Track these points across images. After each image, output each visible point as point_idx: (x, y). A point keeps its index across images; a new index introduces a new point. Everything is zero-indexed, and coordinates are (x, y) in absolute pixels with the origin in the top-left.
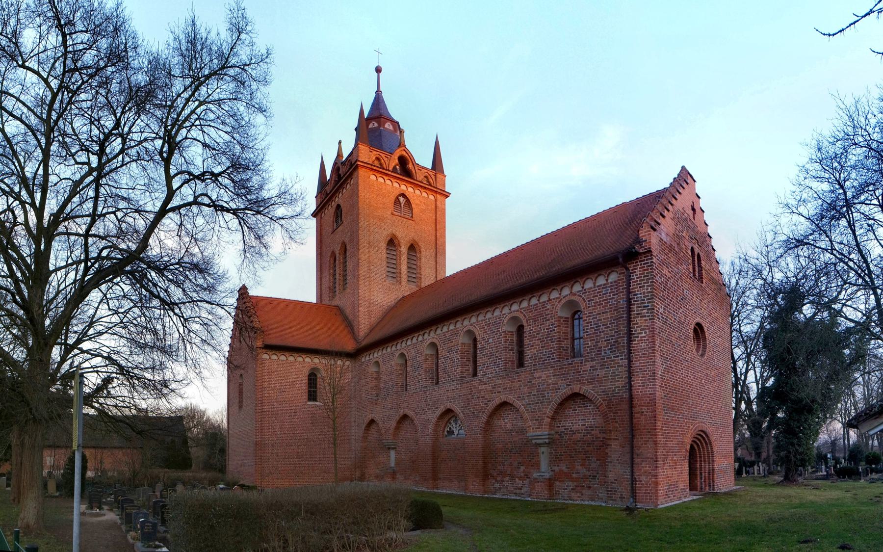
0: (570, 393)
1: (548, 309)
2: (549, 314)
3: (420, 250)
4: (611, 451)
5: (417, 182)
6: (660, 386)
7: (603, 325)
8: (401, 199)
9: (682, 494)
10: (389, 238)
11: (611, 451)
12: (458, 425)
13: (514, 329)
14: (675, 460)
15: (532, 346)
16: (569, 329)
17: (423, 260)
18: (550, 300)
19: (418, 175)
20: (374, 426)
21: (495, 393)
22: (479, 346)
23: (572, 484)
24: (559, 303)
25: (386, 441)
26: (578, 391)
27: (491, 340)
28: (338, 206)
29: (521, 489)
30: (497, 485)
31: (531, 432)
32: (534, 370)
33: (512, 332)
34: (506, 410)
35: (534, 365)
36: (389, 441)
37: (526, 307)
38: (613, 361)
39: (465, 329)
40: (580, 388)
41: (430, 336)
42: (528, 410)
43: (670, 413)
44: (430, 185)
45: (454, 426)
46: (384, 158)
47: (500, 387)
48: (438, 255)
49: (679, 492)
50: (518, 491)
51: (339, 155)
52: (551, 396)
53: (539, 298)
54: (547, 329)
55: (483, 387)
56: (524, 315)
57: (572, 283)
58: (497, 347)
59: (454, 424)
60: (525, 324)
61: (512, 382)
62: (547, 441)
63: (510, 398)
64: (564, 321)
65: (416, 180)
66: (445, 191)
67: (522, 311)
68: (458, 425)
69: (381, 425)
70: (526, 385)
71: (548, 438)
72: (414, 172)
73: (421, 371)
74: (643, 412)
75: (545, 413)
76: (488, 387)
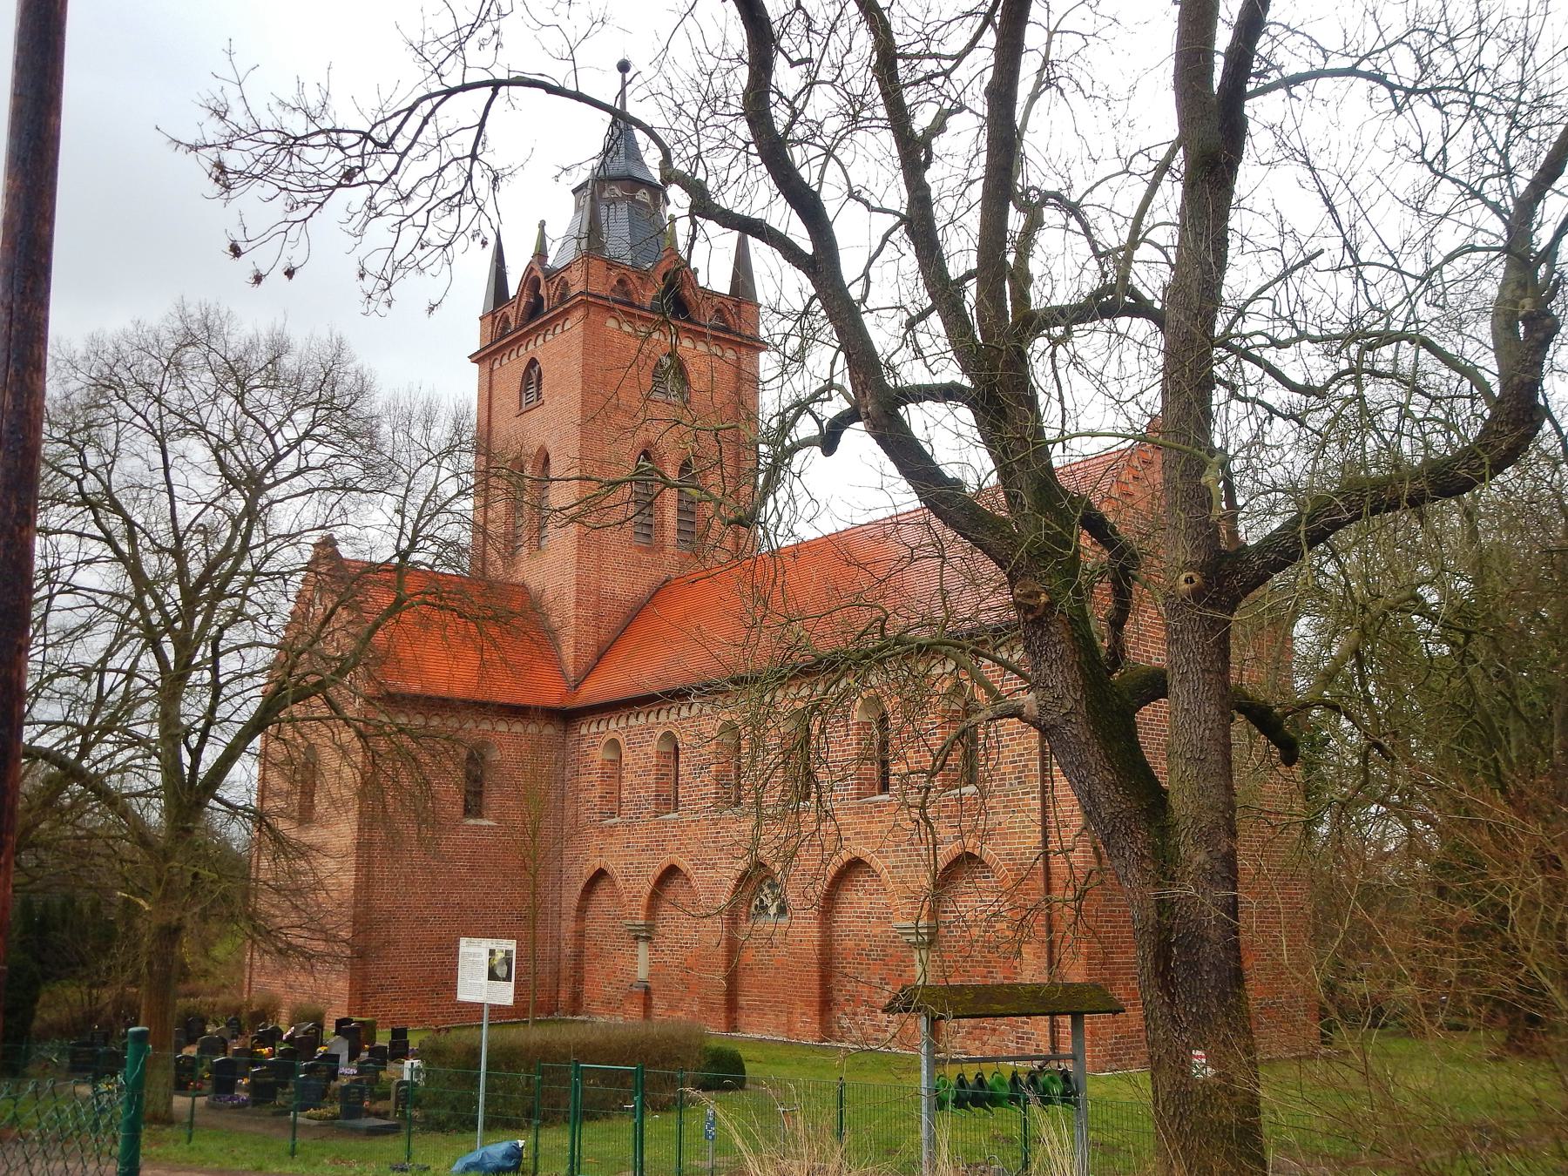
5: (699, 329)
7: (1008, 735)
14: (1132, 989)
20: (603, 884)
28: (533, 362)
29: (886, 1031)
36: (637, 922)
38: (1020, 800)
51: (541, 253)
58: (844, 751)
69: (620, 883)
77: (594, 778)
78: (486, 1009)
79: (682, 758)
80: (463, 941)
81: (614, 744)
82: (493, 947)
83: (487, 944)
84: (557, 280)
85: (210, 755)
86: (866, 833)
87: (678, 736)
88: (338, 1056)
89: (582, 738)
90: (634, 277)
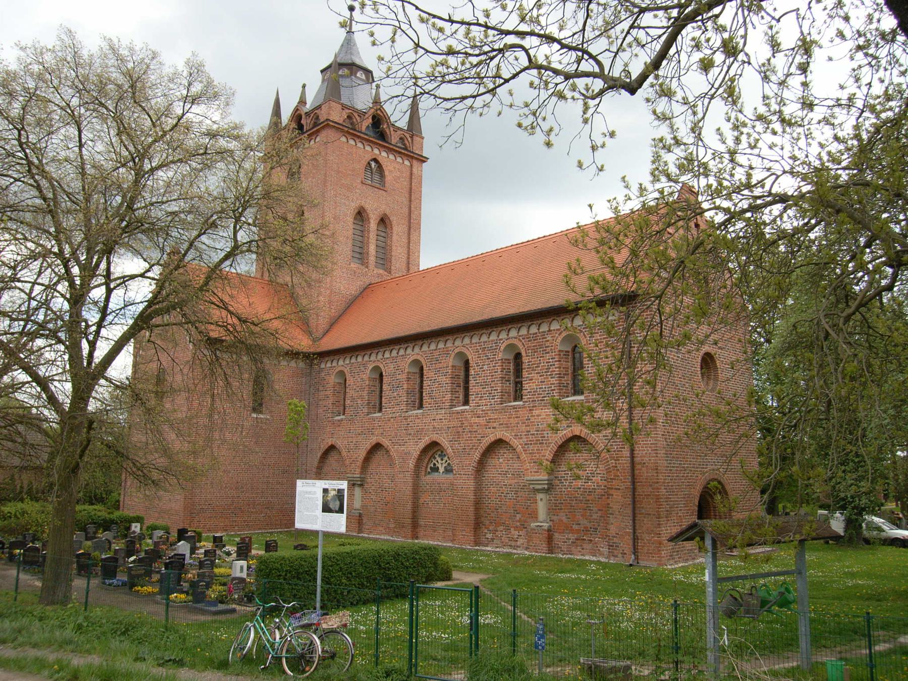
0: (570, 435)
1: (548, 341)
2: (548, 347)
3: (391, 225)
4: (612, 502)
5: (391, 147)
6: (663, 435)
8: (373, 164)
9: (690, 556)
10: (356, 211)
11: (612, 502)
12: (444, 461)
13: (511, 357)
14: (680, 516)
15: (532, 380)
16: (569, 364)
17: (395, 237)
18: (550, 331)
19: (393, 138)
21: (490, 428)
22: (472, 372)
23: (572, 537)
24: (559, 335)
25: (352, 475)
26: (578, 434)
27: (485, 367)
30: (489, 536)
31: (528, 476)
32: (533, 407)
33: (509, 360)
34: (501, 448)
35: (533, 401)
36: (355, 476)
37: (525, 335)
39: (456, 351)
40: (581, 430)
41: (414, 353)
42: (526, 450)
43: (674, 463)
44: (406, 149)
45: (439, 461)
46: (357, 117)
47: (495, 422)
48: (412, 230)
49: (685, 554)
50: (513, 543)
51: (302, 102)
52: (551, 437)
53: (539, 326)
54: (547, 362)
55: (477, 420)
56: (523, 344)
57: (573, 315)
58: (492, 376)
59: (439, 459)
60: (523, 354)
61: (509, 418)
62: (546, 486)
63: (506, 435)
64: (564, 355)
65: (391, 144)
66: (422, 156)
67: (521, 338)
68: (444, 461)
69: (344, 453)
70: (525, 423)
71: (547, 484)
72: (388, 133)
73: (403, 393)
74: (644, 463)
75: (545, 456)
76: (482, 421)
77: (328, 393)
78: (320, 536)
79: (385, 380)
80: (299, 483)
81: (341, 374)
82: (326, 487)
83: (321, 484)
84: (312, 115)
85: (102, 349)
86: (507, 424)
87: (383, 369)
88: (185, 555)
89: (321, 370)
90: (356, 115)
